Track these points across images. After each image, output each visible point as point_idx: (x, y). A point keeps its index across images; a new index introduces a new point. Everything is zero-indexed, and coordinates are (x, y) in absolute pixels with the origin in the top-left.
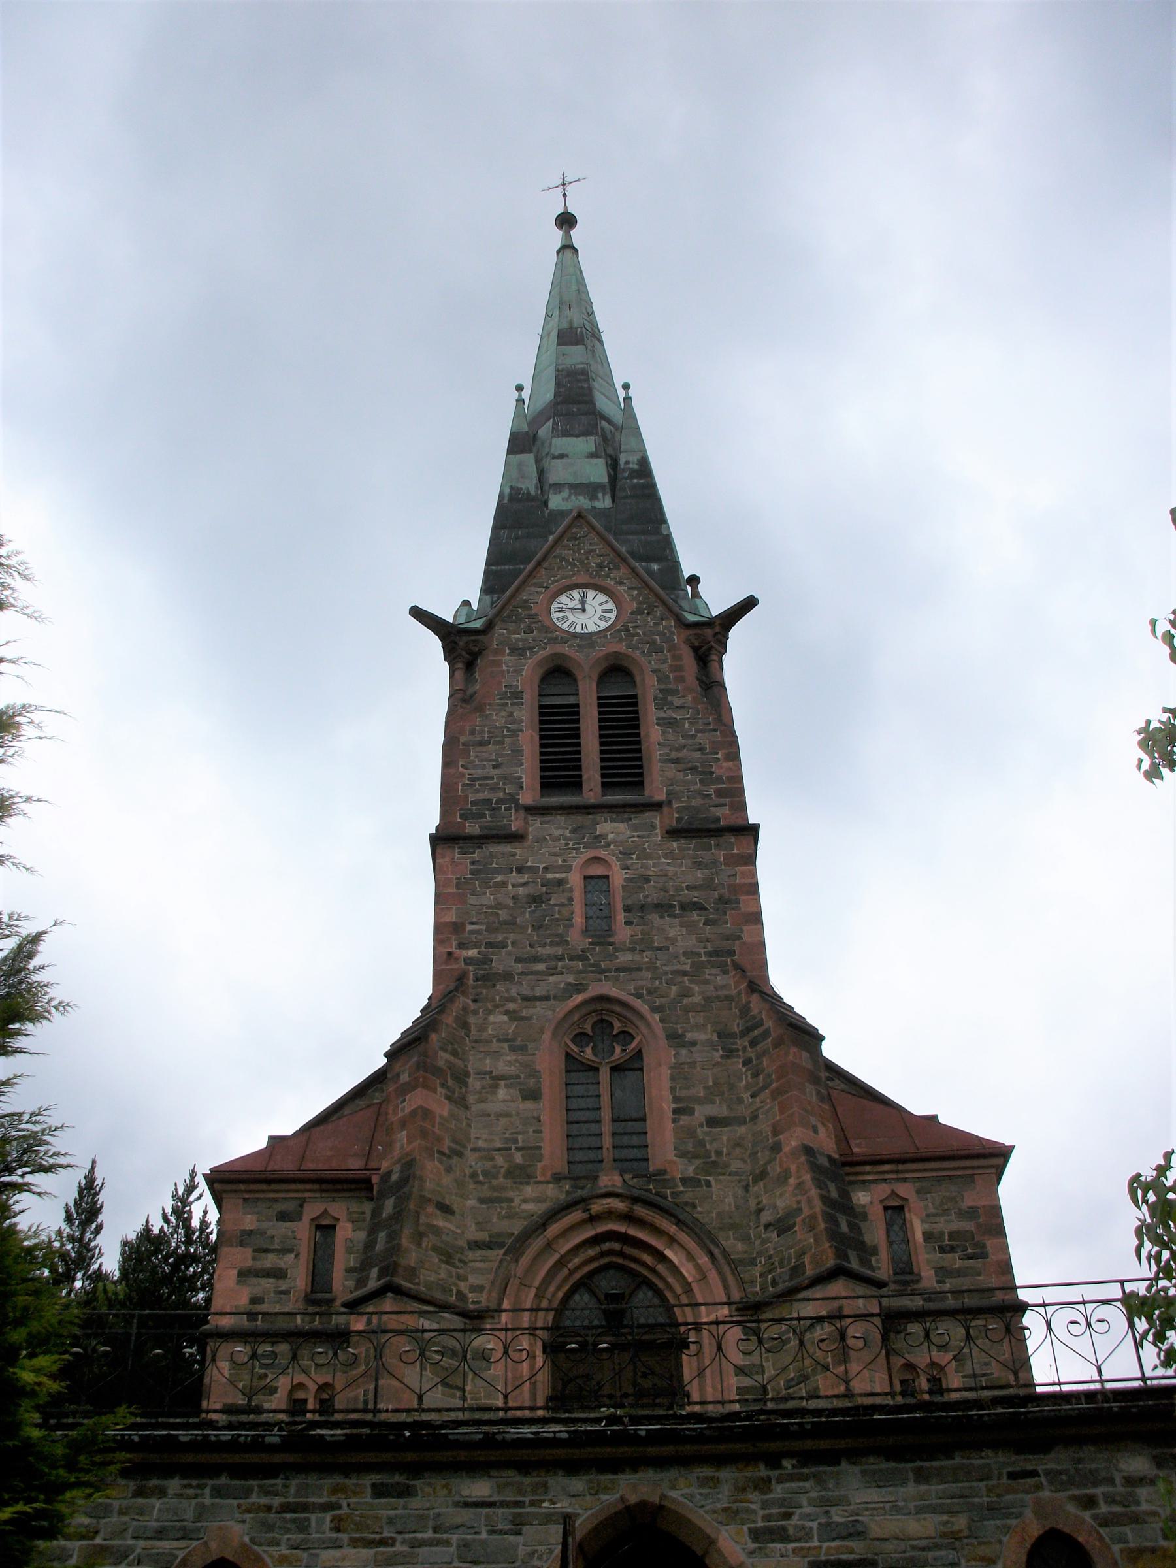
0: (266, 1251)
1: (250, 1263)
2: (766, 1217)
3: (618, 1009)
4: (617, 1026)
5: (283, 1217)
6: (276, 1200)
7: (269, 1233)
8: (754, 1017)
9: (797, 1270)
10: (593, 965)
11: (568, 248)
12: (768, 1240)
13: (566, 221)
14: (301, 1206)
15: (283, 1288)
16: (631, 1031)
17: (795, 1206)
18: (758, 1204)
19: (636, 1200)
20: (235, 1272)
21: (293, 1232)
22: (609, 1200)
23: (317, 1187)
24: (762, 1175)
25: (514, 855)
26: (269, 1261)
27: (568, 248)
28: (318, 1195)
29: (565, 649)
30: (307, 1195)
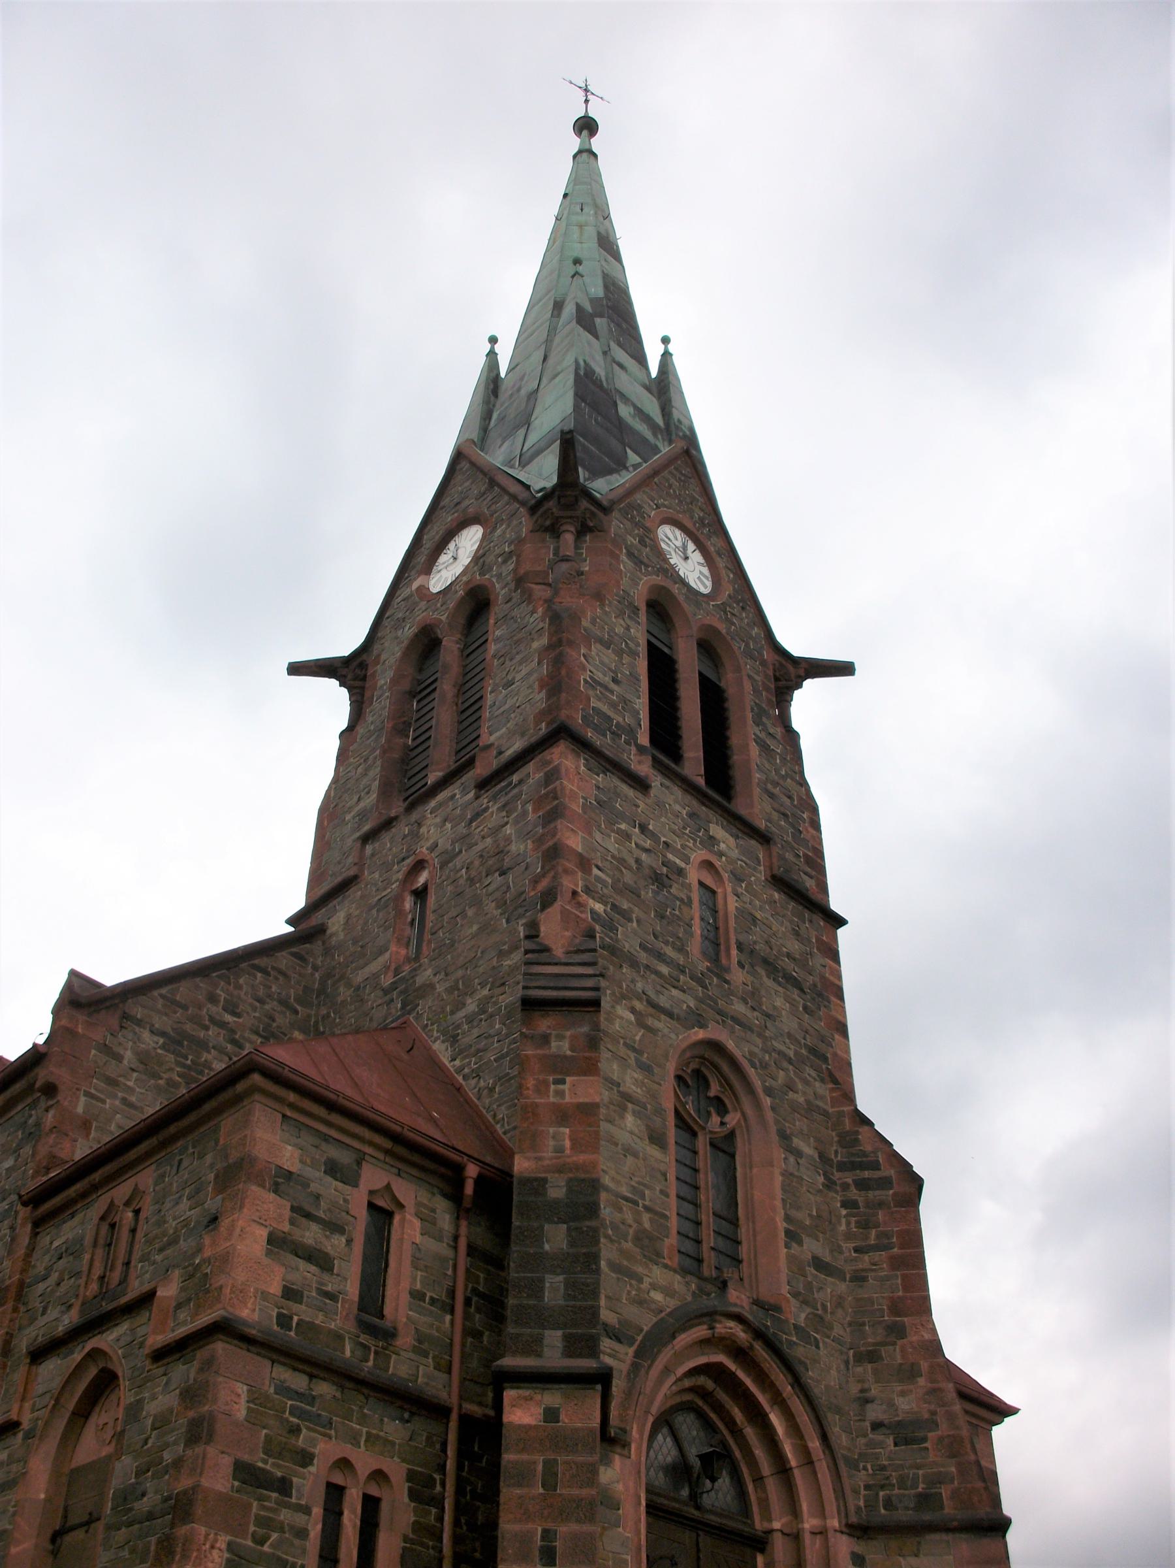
0: (308, 1216)
1: (286, 1227)
2: (875, 1412)
3: (725, 1068)
4: (714, 1090)
5: (332, 1169)
6: (326, 1138)
7: (314, 1187)
8: (864, 1154)
9: (926, 1500)
10: (710, 998)
11: (586, 155)
12: (881, 1445)
13: (586, 126)
14: (359, 1163)
15: (329, 1288)
16: (727, 1101)
17: (926, 1416)
18: (862, 1391)
19: (759, 1334)
20: (263, 1233)
21: (345, 1201)
22: (731, 1324)
23: (387, 1144)
24: (872, 1356)
25: (637, 806)
26: (311, 1234)
27: (586, 155)
28: (381, 1156)
29: (675, 589)
30: (369, 1150)
